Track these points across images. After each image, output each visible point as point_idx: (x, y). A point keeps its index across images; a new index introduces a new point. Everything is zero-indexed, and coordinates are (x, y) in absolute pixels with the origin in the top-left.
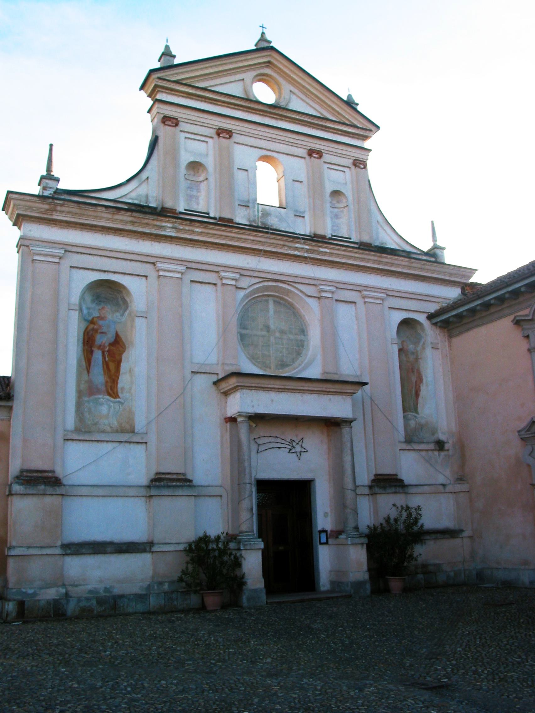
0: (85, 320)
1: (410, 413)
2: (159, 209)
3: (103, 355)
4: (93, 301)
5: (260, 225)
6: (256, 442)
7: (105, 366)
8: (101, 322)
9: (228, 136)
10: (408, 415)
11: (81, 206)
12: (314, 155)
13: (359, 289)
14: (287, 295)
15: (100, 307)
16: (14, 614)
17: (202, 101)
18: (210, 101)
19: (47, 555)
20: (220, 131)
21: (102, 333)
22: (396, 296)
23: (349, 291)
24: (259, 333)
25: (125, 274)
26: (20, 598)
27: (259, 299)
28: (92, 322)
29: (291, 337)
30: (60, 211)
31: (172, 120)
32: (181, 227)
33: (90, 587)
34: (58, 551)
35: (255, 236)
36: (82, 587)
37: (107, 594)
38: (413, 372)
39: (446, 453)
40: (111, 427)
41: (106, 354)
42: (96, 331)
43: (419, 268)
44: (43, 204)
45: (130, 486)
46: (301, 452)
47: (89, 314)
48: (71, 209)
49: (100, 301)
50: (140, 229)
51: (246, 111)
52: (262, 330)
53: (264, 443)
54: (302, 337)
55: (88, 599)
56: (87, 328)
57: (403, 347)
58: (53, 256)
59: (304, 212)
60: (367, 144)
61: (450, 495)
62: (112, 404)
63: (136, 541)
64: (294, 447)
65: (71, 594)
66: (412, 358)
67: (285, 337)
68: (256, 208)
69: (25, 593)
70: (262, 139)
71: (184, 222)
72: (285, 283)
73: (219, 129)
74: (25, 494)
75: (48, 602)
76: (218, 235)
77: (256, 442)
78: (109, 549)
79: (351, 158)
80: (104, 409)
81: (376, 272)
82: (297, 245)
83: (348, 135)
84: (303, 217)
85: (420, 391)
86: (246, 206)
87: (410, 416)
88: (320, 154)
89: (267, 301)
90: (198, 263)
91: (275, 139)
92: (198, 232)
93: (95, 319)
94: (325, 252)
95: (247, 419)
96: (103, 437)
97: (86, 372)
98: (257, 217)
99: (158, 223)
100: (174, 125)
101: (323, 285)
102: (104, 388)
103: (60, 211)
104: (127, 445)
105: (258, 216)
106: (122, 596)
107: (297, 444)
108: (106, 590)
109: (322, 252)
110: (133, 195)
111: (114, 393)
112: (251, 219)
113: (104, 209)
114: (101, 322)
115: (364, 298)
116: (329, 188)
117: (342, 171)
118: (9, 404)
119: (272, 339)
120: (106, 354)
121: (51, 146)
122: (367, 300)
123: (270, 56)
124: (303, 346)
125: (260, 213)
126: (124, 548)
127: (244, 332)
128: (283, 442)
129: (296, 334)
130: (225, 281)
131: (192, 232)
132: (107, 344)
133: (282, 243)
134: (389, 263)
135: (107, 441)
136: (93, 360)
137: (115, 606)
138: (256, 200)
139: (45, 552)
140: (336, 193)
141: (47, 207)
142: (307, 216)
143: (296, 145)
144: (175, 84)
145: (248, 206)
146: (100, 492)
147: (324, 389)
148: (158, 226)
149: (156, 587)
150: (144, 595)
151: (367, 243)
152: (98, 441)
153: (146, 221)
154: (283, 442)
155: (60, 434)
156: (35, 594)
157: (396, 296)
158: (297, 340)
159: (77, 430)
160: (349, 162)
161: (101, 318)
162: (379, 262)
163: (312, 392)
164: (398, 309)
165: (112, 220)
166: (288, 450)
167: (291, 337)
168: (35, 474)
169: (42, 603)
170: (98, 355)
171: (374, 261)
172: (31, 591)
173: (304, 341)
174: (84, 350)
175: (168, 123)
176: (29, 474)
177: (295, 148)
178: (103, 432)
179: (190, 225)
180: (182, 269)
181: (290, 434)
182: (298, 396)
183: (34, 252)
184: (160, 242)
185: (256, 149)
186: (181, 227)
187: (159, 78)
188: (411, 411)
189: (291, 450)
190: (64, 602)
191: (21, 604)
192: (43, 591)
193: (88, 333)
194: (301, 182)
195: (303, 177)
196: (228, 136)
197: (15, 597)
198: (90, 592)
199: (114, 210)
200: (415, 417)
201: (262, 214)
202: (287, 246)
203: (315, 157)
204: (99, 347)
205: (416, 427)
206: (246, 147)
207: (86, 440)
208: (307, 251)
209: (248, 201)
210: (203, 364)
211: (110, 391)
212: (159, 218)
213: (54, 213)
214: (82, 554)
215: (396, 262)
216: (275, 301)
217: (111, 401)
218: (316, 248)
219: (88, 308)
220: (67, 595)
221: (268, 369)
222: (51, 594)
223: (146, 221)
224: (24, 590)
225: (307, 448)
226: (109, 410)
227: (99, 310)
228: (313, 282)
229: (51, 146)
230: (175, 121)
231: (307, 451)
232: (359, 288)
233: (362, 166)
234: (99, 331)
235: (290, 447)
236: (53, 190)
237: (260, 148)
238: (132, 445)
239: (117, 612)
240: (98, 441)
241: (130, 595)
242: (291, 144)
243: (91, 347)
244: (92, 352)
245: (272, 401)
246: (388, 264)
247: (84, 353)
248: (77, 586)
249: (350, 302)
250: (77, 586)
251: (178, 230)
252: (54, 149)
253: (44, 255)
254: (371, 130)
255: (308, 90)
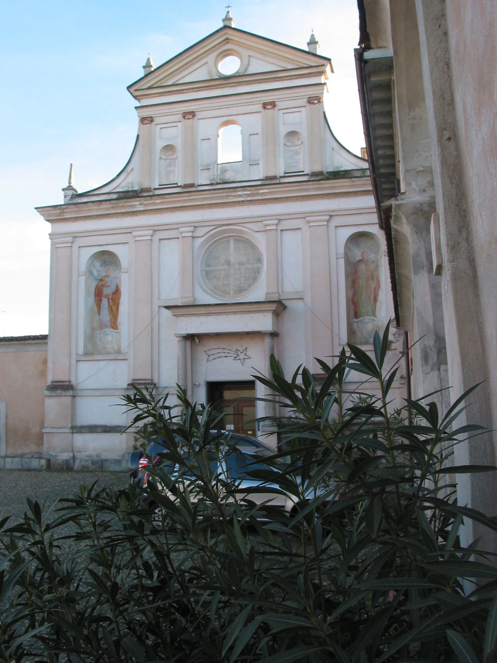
0: (96, 279)
1: (367, 317)
2: (139, 190)
3: (109, 302)
4: (101, 266)
5: (218, 181)
6: (206, 354)
7: (110, 309)
8: (107, 279)
9: (191, 117)
10: (365, 319)
11: (78, 205)
12: (267, 107)
13: (303, 216)
14: (242, 234)
15: (106, 269)
16: (45, 466)
17: (172, 94)
18: (177, 92)
19: (62, 432)
20: (184, 115)
21: (108, 286)
22: (344, 215)
23: (294, 220)
24: (221, 268)
25: (107, 245)
26: (48, 457)
27: (221, 241)
28: (101, 280)
29: (249, 266)
30: (67, 212)
31: (147, 119)
32: (145, 203)
33: (87, 453)
34: (68, 430)
35: (202, 195)
36: (83, 453)
37: (98, 458)
38: (373, 279)
39: (394, 352)
40: (114, 350)
41: (110, 300)
42: (103, 286)
43: (364, 184)
44: (56, 210)
45: (116, 389)
46: (244, 359)
47: (99, 275)
48: (73, 209)
49: (106, 265)
50: (119, 211)
51: (208, 89)
52: (223, 265)
53: (214, 354)
54: (259, 265)
55: (86, 461)
56: (97, 285)
57: (363, 258)
58: (67, 243)
59: (258, 160)
60: (323, 80)
61: (396, 390)
62: (114, 334)
63: (121, 425)
64: (238, 355)
65: (77, 457)
66: (372, 267)
67: (243, 267)
68: (216, 167)
69: (51, 455)
70: (221, 108)
71: (146, 199)
72: (235, 225)
73: (184, 113)
74: (51, 396)
75: (63, 461)
76: (179, 200)
77: (206, 354)
78: (98, 430)
79: (305, 97)
80: (110, 338)
81: (322, 197)
82: (239, 193)
83: (304, 76)
84: (258, 164)
85: (378, 296)
86: (208, 169)
87: (367, 320)
88: (273, 104)
89: (228, 241)
90: (164, 225)
91: (233, 104)
92: (158, 203)
93: (103, 278)
94: (265, 193)
95: (182, 339)
96: (99, 357)
97: (97, 314)
98: (216, 176)
99: (129, 204)
100: (150, 122)
101: (265, 220)
102: (109, 324)
103: (67, 212)
104: (116, 362)
105: (217, 175)
106: (106, 460)
107: (241, 352)
108: (97, 456)
109: (262, 193)
110: (123, 184)
111: (115, 326)
112: (212, 179)
113: (91, 204)
114: (107, 279)
115: (309, 222)
116: (283, 130)
117: (299, 111)
118: (46, 341)
119: (232, 271)
120: (110, 300)
121: (71, 164)
122: (311, 224)
123: (226, 34)
124: (258, 272)
125: (219, 171)
126: (108, 429)
127: (208, 269)
128: (229, 352)
129: (253, 264)
130: (184, 235)
131: (154, 204)
132: (111, 294)
133: (225, 194)
134: (331, 187)
135: (103, 360)
136: (102, 305)
137: (102, 466)
138: (216, 161)
139: (61, 431)
140: (292, 134)
141: (58, 211)
142: (261, 162)
143: (252, 103)
144: (149, 90)
145: (209, 169)
146: (98, 393)
147: (244, 310)
148: (129, 206)
149: (127, 456)
150: (120, 460)
151: (318, 172)
152: (98, 360)
153: (120, 205)
154: (229, 352)
155: (74, 357)
156: (56, 456)
157: (344, 215)
158: (253, 268)
159: (86, 354)
160: (304, 102)
161: (106, 276)
162: (320, 189)
163: (235, 313)
164: (346, 226)
165: (100, 209)
166: (233, 358)
167: (249, 266)
168: (59, 384)
169: (60, 461)
170: (105, 302)
171: (314, 189)
172: (54, 454)
173: (260, 268)
174: (96, 300)
175: (146, 122)
176: (55, 384)
177: (253, 106)
178: (109, 353)
179: (151, 200)
180: (151, 232)
181: (236, 345)
182: (224, 317)
183: (56, 242)
184: (137, 216)
185: (218, 118)
186: (145, 203)
187: (136, 90)
188: (368, 315)
189: (236, 357)
190: (72, 461)
191: (49, 461)
192: (61, 454)
193: (98, 288)
194: (257, 134)
195: (258, 129)
196: (191, 117)
197: (46, 457)
198: (88, 456)
199: (98, 202)
200: (373, 320)
201: (221, 172)
202: (231, 196)
203: (268, 109)
204: (106, 296)
205: (373, 329)
206: (209, 120)
207: (91, 360)
208: (248, 195)
209: (209, 165)
210: (166, 300)
211: (113, 325)
212: (128, 200)
213: (64, 214)
214: (82, 433)
215: (336, 185)
216: (235, 240)
217: (113, 332)
218: (255, 192)
219: (98, 271)
220: (74, 458)
221: (228, 295)
222: (65, 456)
223: (120, 205)
224: (51, 453)
225: (250, 356)
226: (113, 338)
227: (106, 271)
228: (259, 219)
229: (71, 164)
230: (149, 119)
231: (250, 358)
232: (303, 216)
233: (316, 102)
234: (106, 285)
235: (235, 356)
236: (70, 197)
237: (221, 117)
238: (119, 362)
239: (103, 470)
240: (98, 360)
241: (111, 460)
242: (248, 104)
243: (100, 297)
244: (101, 300)
245: (202, 323)
246: (330, 188)
247: (96, 302)
248: (80, 452)
249: (297, 229)
250: (80, 452)
251: (145, 205)
252: (73, 166)
253: (61, 243)
254: (323, 65)
255: (263, 50)
